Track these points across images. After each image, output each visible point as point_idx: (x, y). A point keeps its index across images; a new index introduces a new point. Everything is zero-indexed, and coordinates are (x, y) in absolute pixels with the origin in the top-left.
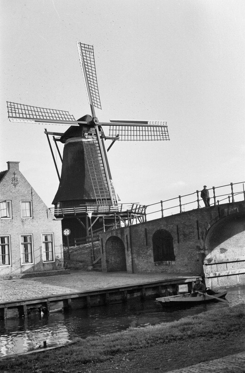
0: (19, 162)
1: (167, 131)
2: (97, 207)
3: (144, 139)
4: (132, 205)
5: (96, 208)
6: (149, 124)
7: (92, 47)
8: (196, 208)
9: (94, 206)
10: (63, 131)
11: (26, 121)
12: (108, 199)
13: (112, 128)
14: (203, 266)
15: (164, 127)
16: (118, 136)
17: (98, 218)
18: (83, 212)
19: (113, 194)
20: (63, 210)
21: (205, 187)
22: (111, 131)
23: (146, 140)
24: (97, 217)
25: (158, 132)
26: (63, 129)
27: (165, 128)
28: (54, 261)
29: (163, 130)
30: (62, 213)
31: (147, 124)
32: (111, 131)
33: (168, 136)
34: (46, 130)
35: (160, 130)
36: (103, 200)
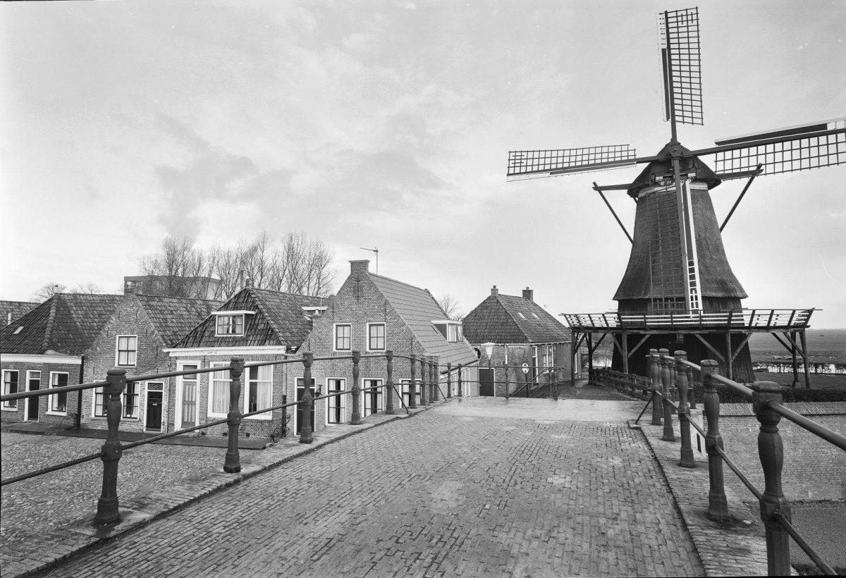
2: (728, 314)
6: (830, 128)
7: (694, 11)
10: (630, 181)
11: (517, 177)
12: (678, 299)
14: (109, 427)
16: (759, 166)
17: (647, 336)
18: (690, 325)
19: (691, 290)
20: (675, 318)
21: (495, 287)
22: (686, 120)
24: (645, 335)
26: (630, 174)
27: (669, 15)
28: (51, 372)
30: (643, 320)
31: (826, 128)
34: (595, 183)
36: (666, 299)
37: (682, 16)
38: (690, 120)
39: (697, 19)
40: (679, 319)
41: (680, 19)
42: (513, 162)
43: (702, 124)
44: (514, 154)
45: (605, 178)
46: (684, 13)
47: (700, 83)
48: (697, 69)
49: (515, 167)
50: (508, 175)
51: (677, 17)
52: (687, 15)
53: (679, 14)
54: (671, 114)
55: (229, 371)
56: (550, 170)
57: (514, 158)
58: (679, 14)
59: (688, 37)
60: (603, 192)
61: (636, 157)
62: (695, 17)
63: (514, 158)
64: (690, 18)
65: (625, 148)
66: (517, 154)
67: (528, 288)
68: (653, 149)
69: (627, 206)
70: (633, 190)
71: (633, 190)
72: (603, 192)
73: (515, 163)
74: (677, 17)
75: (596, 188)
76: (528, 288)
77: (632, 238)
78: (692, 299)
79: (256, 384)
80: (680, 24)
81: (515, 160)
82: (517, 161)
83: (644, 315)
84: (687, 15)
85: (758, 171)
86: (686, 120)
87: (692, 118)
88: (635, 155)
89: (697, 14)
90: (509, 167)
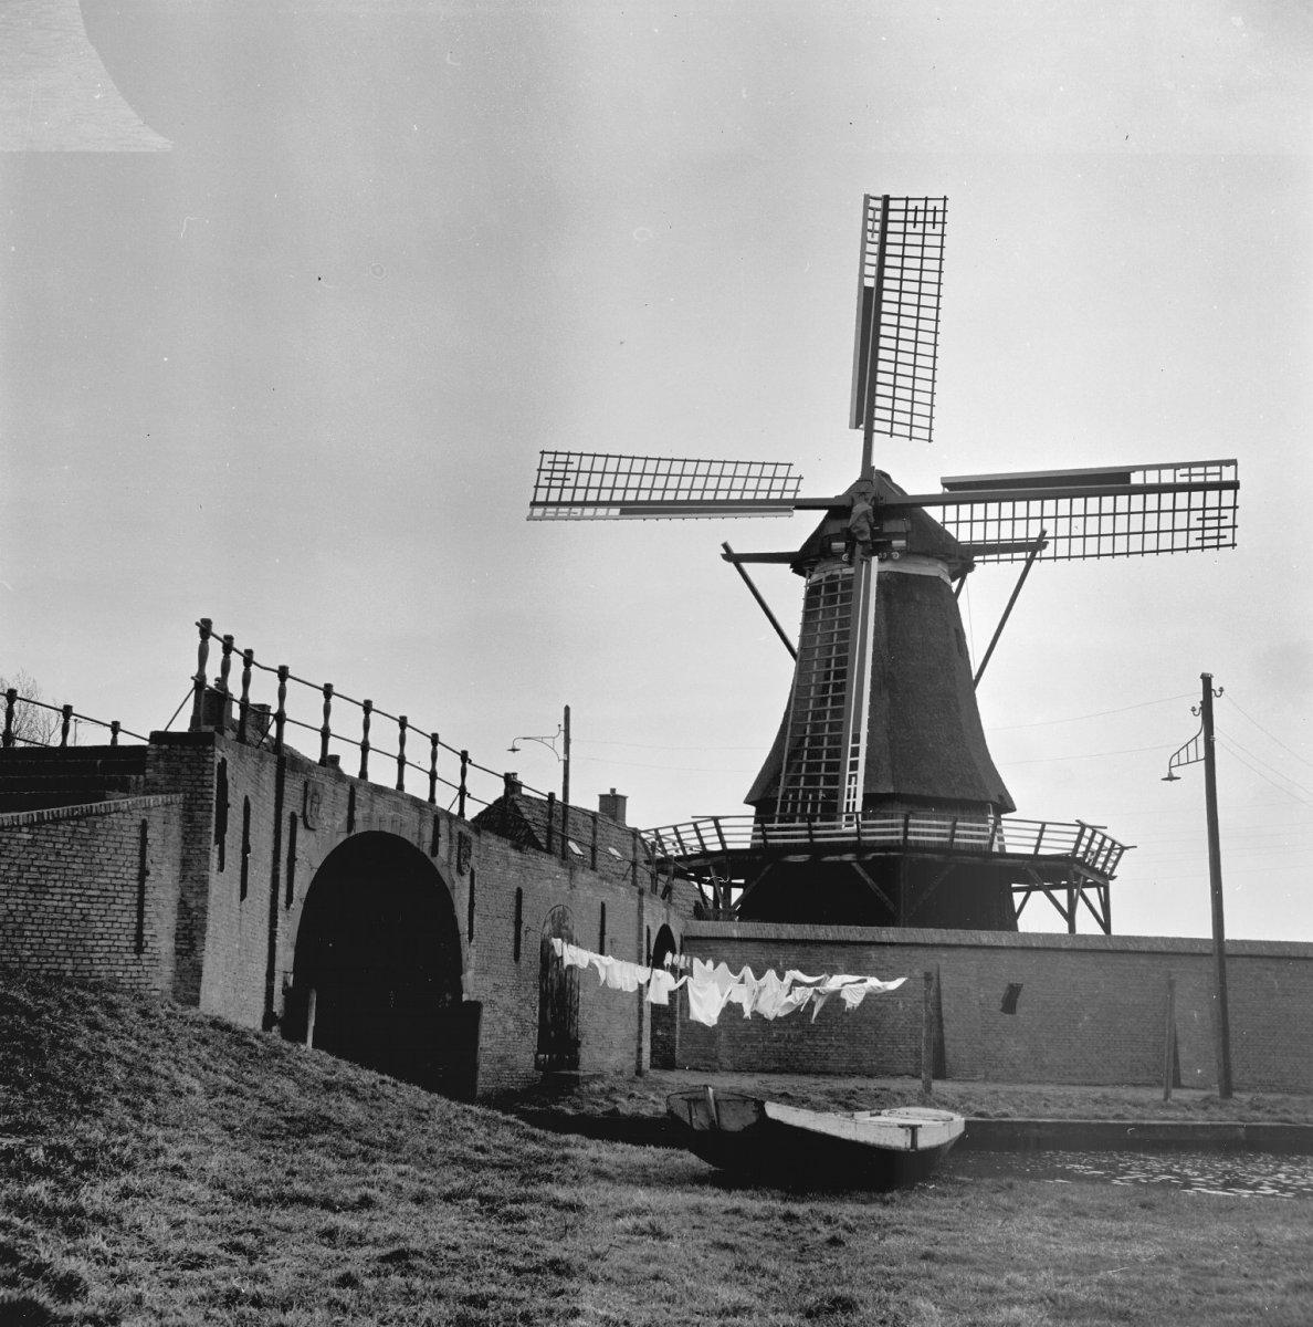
8: (108, 743)
13: (886, 427)
19: (850, 776)
22: (897, 429)
26: (799, 529)
27: (892, 205)
33: (926, 199)
34: (725, 546)
37: (916, 210)
38: (905, 430)
39: (944, 223)
40: (826, 833)
41: (911, 216)
42: (548, 474)
43: (930, 441)
44: (551, 458)
46: (921, 205)
47: (934, 369)
48: (929, 350)
49: (550, 487)
50: (534, 504)
51: (906, 210)
52: (925, 222)
53: (912, 205)
54: (864, 415)
57: (1200, 524)
58: (912, 205)
59: (921, 270)
60: (745, 565)
61: (799, 496)
62: (939, 217)
63: (550, 467)
64: (930, 217)
65: (782, 471)
66: (560, 458)
68: (836, 481)
69: (788, 591)
70: (800, 562)
71: (800, 562)
72: (745, 565)
73: (1219, 518)
75: (729, 556)
76: (613, 790)
77: (796, 644)
78: (849, 797)
80: (910, 228)
82: (556, 475)
84: (925, 211)
86: (897, 429)
87: (892, 422)
88: (797, 491)
89: (944, 211)
90: (537, 487)
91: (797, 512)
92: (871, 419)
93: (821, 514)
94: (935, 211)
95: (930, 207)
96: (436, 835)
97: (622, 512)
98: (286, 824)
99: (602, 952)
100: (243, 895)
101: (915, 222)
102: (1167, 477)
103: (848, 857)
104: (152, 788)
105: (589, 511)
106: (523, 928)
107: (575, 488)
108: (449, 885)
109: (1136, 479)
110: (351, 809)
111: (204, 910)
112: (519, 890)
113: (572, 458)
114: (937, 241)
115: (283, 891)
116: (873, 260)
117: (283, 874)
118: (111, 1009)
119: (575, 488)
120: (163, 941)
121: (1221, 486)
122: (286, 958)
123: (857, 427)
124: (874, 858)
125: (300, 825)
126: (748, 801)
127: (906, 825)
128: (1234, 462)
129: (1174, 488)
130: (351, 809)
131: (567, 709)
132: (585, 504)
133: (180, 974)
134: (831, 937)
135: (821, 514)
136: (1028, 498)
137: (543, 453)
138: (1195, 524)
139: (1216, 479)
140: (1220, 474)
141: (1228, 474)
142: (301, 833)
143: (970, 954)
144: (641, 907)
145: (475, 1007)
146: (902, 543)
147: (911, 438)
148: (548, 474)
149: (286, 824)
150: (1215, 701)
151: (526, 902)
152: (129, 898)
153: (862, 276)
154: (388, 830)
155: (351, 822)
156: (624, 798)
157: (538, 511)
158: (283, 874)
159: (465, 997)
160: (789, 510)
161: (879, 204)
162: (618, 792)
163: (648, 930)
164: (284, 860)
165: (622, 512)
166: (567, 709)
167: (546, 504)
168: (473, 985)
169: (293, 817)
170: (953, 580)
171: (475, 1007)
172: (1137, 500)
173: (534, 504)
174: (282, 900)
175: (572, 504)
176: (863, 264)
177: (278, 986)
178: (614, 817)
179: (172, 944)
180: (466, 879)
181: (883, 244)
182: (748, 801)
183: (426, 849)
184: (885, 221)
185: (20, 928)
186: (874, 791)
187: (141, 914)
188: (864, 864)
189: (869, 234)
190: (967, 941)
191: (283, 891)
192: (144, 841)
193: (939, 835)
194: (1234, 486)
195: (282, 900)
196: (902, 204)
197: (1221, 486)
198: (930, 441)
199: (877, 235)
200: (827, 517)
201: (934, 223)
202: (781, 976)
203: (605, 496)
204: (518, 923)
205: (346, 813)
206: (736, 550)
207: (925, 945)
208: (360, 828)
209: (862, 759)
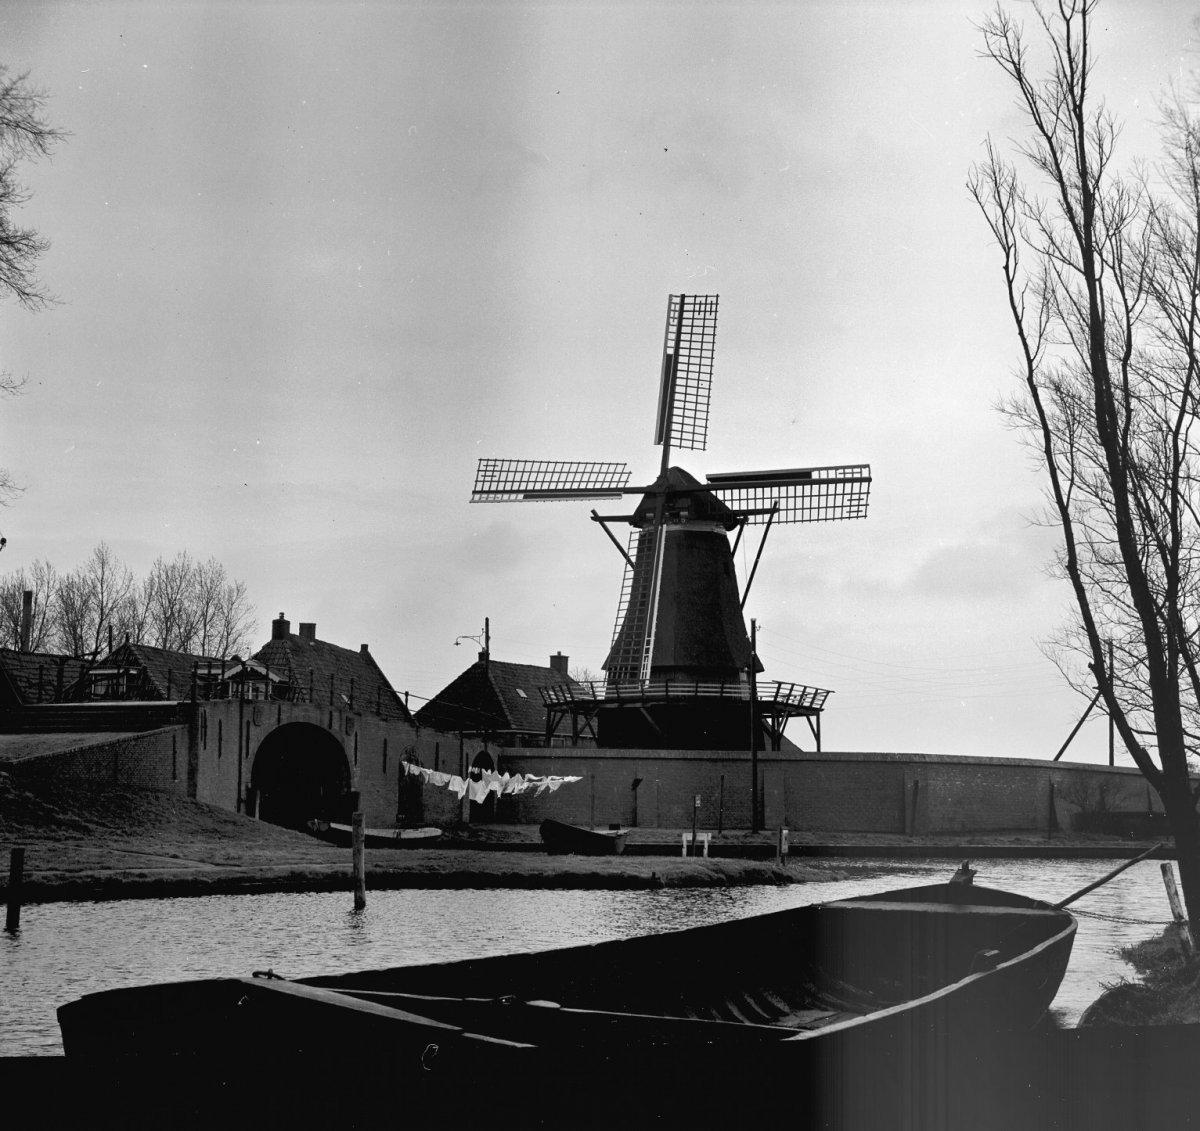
0: (282, 614)
1: (696, 297)
3: (702, 431)
4: (777, 685)
5: (663, 687)
9: (659, 682)
13: (677, 442)
15: (682, 304)
22: (684, 443)
23: (715, 327)
25: (696, 323)
26: (631, 504)
27: (687, 300)
29: (691, 307)
31: (810, 477)
32: (684, 443)
33: (707, 296)
34: (593, 512)
35: (690, 315)
37: (700, 304)
38: (689, 444)
39: (716, 311)
42: (483, 473)
43: (704, 449)
44: (485, 463)
45: (606, 507)
51: (695, 304)
52: (705, 311)
53: (698, 300)
54: (664, 436)
55: (815, 750)
56: (525, 491)
58: (698, 300)
60: (607, 524)
62: (714, 307)
65: (620, 469)
66: (490, 463)
67: (559, 653)
68: (648, 476)
71: (634, 520)
72: (607, 524)
74: (695, 304)
75: (596, 517)
76: (559, 653)
79: (679, 854)
81: (486, 471)
83: (696, 696)
84: (706, 304)
85: (774, 510)
88: (626, 482)
89: (717, 304)
90: (477, 481)
91: (625, 496)
92: (668, 438)
93: (640, 497)
94: (711, 304)
95: (709, 301)
96: (331, 720)
97: (525, 497)
98: (244, 725)
99: (436, 769)
100: (220, 755)
101: (699, 311)
102: (832, 475)
103: (638, 705)
104: (178, 723)
105: (506, 497)
106: (388, 758)
107: (499, 481)
108: (340, 740)
109: (815, 475)
110: (279, 715)
111: (197, 764)
112: (385, 740)
113: (497, 463)
114: (712, 323)
115: (244, 751)
116: (674, 329)
117: (244, 743)
118: (157, 798)
119: (499, 481)
120: (183, 775)
121: (861, 480)
122: (247, 776)
123: (659, 444)
124: (652, 706)
125: (252, 723)
126: (603, 668)
127: (667, 687)
128: (868, 466)
129: (836, 481)
130: (279, 715)
131: (487, 620)
132: (504, 492)
133: (189, 786)
134: (579, 755)
135: (640, 497)
136: (755, 487)
137: (480, 460)
138: (847, 503)
139: (858, 476)
140: (861, 472)
141: (865, 473)
142: (252, 728)
143: (654, 762)
144: (462, 743)
145: (357, 795)
146: (686, 513)
147: (692, 449)
148: (483, 473)
149: (244, 725)
150: (757, 633)
151: (389, 745)
152: (171, 761)
153: (666, 347)
154: (301, 721)
155: (279, 720)
156: (566, 658)
157: (477, 497)
158: (244, 743)
159: (353, 790)
160: (620, 495)
161: (678, 300)
162: (562, 654)
163: (467, 755)
164: (244, 738)
165: (525, 497)
166: (487, 620)
167: (482, 492)
168: (356, 784)
169: (248, 723)
170: (730, 528)
171: (357, 795)
172: (816, 487)
173: (475, 492)
174: (244, 755)
175: (497, 492)
176: (667, 339)
177: (243, 788)
178: (559, 671)
179: (187, 776)
180: (353, 738)
181: (680, 326)
182: (603, 668)
183: (325, 726)
184: (682, 311)
185: (132, 774)
186: (659, 664)
187: (174, 766)
188: (646, 709)
189: (671, 320)
190: (541, 754)
191: (244, 751)
192: (174, 742)
193: (689, 692)
194: (869, 480)
195: (244, 755)
196: (691, 300)
197: (861, 480)
198: (704, 449)
199: (676, 321)
200: (644, 498)
201: (711, 311)
202: (524, 777)
203: (515, 487)
204: (385, 755)
205: (277, 716)
206: (601, 514)
207: (538, 757)
208: (284, 721)
209: (651, 647)
